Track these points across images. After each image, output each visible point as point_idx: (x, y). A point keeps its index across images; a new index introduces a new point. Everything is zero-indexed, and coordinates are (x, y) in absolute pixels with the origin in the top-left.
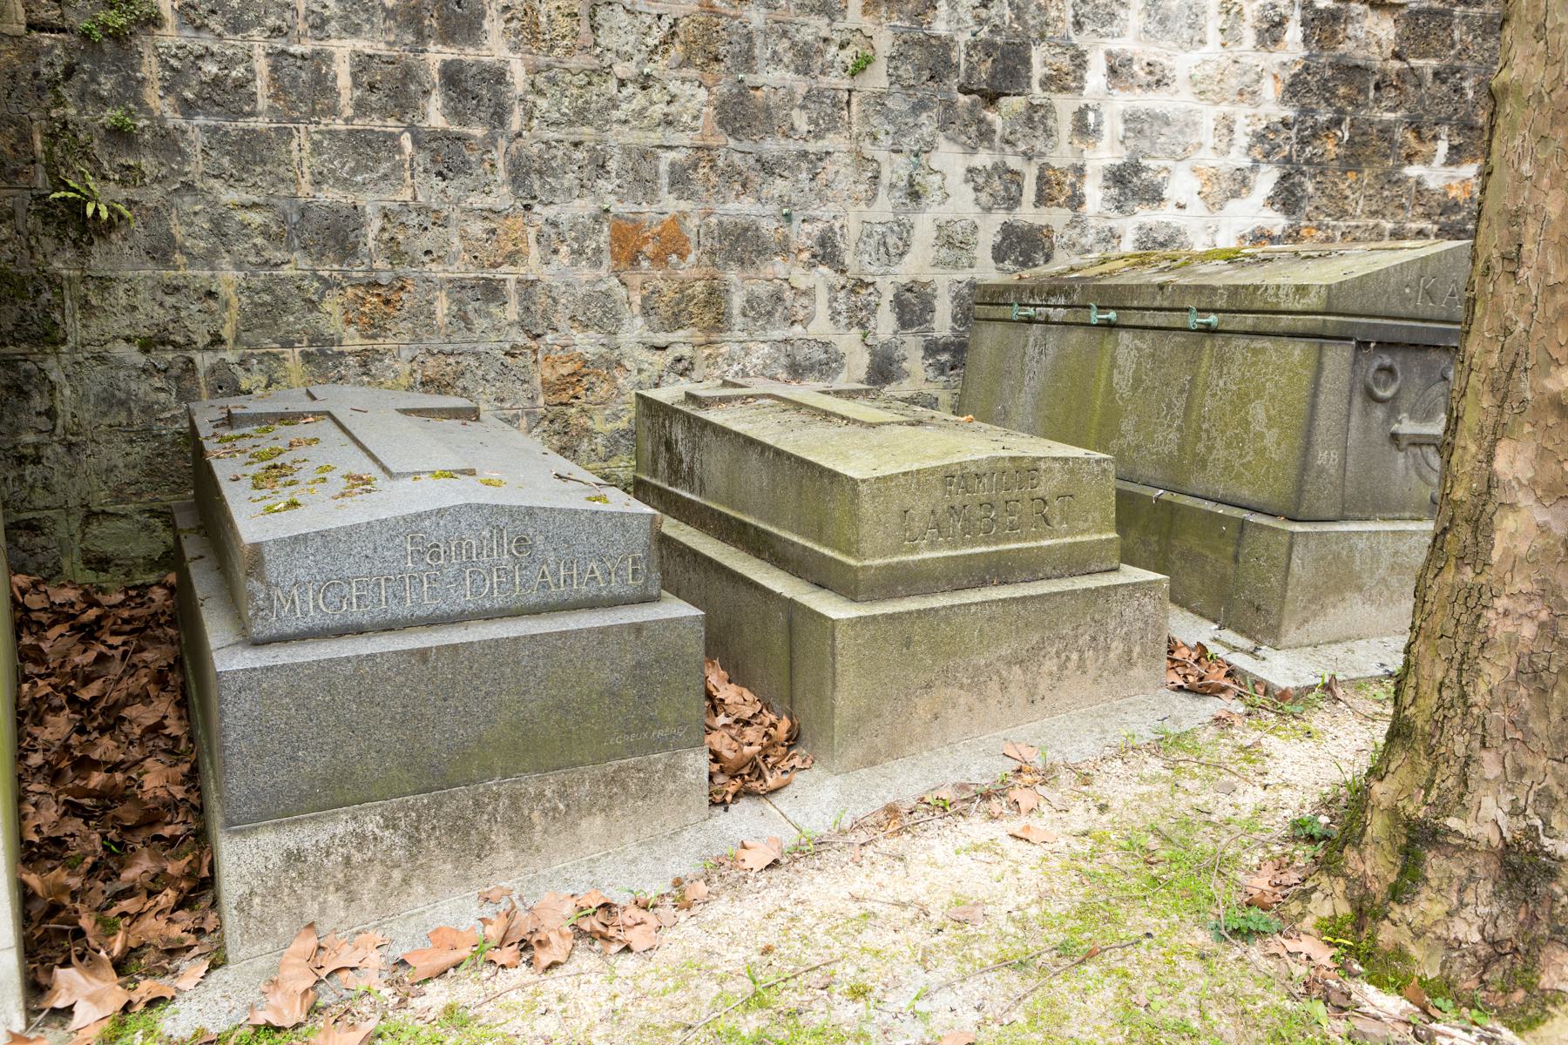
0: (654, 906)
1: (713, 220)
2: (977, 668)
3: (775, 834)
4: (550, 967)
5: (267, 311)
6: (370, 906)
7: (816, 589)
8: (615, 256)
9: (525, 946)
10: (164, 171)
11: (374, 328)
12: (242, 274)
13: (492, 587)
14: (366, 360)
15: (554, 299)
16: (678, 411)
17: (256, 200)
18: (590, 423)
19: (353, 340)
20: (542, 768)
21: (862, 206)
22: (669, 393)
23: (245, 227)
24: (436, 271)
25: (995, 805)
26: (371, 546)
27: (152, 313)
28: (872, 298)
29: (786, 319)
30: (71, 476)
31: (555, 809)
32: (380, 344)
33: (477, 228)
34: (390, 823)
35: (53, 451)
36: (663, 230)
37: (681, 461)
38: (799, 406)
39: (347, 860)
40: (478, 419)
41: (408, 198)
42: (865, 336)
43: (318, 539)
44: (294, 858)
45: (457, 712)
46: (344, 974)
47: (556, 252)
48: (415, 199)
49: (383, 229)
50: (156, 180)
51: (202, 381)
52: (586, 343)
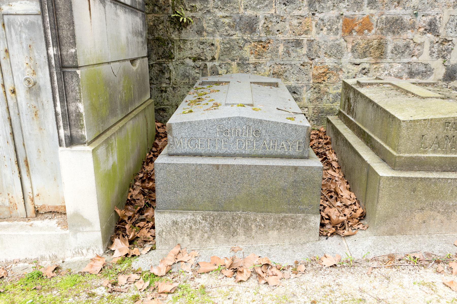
0: (283, 270)
1: (384, 17)
2: (448, 206)
3: (341, 253)
4: (241, 281)
5: (228, 50)
6: (197, 243)
7: (382, 161)
8: (343, 31)
9: (235, 271)
10: (202, 7)
11: (259, 55)
12: (221, 38)
13: (245, 146)
14: (256, 65)
15: (320, 47)
16: (352, 88)
17: (227, 15)
18: (328, 90)
19: (252, 59)
20: (257, 211)
21: (451, 9)
22: (351, 82)
23: (223, 23)
24: (280, 37)
25: (441, 267)
26: (205, 128)
27: (197, 50)
28: (450, 46)
29: (410, 55)
30: (174, 97)
31: (260, 225)
32: (261, 61)
33: (295, 22)
34: (205, 219)
35: (170, 89)
36: (363, 21)
37: (351, 106)
38: (398, 88)
39: (191, 227)
40: (277, 86)
41: (273, 13)
42: (444, 62)
43: (189, 124)
44: (175, 223)
45: (228, 187)
46: (183, 263)
47: (322, 30)
48: (275, 13)
49: (265, 23)
50: (200, 10)
51: (209, 71)
52: (329, 62)
